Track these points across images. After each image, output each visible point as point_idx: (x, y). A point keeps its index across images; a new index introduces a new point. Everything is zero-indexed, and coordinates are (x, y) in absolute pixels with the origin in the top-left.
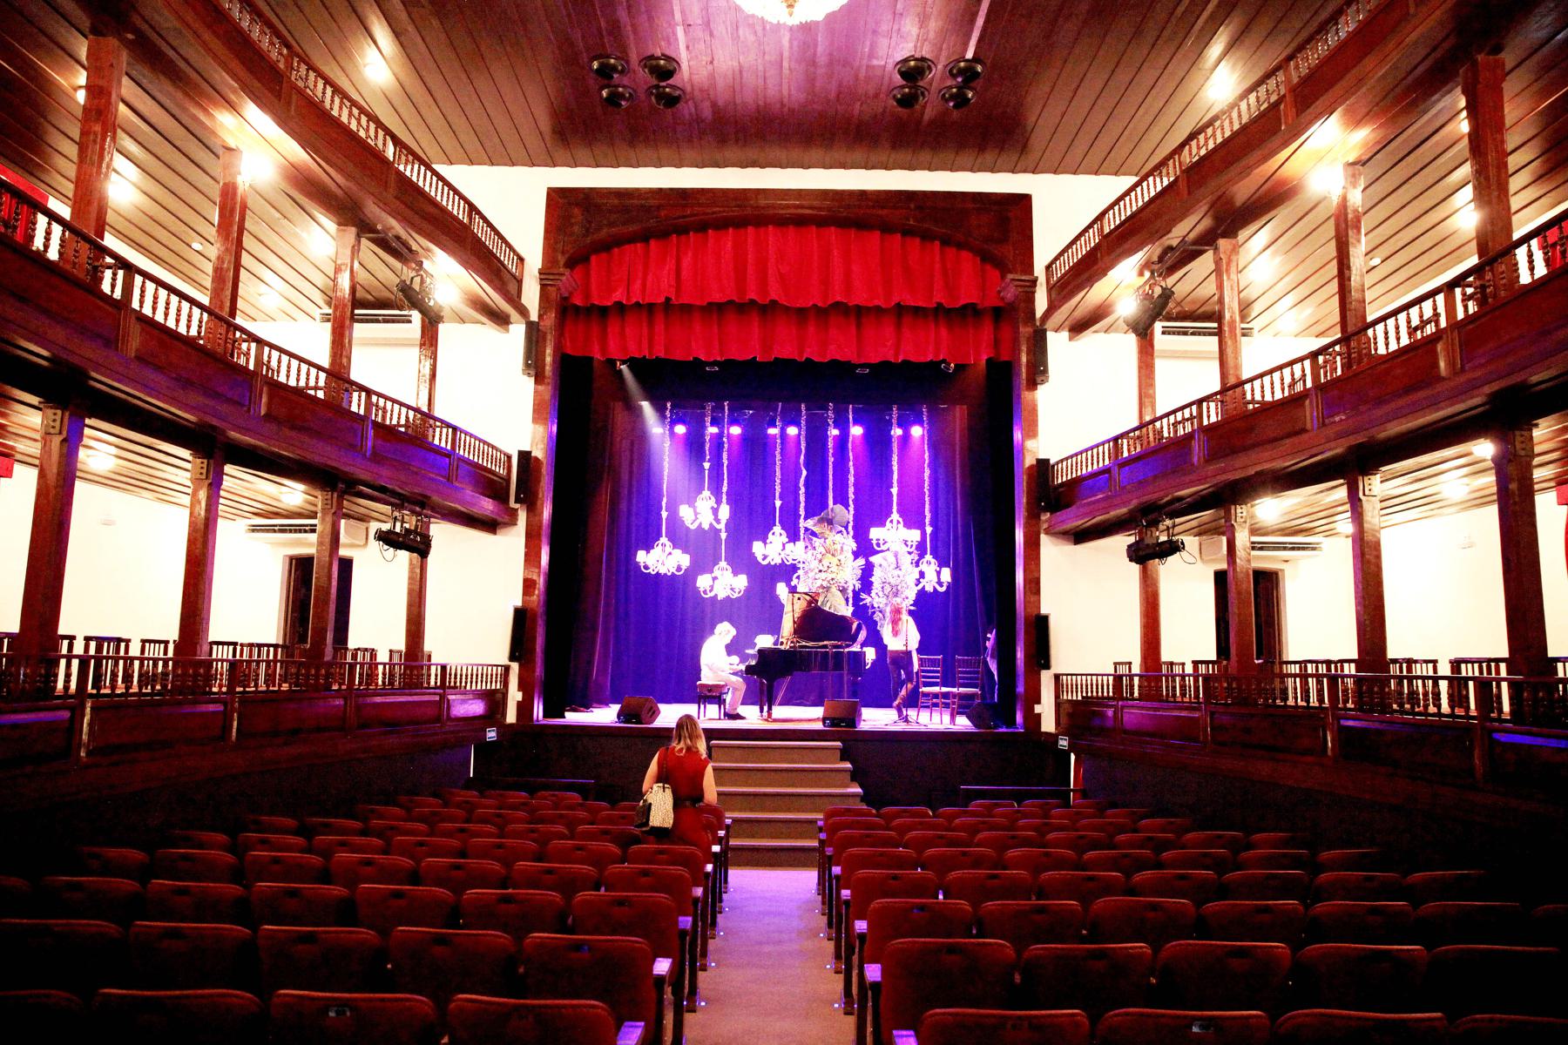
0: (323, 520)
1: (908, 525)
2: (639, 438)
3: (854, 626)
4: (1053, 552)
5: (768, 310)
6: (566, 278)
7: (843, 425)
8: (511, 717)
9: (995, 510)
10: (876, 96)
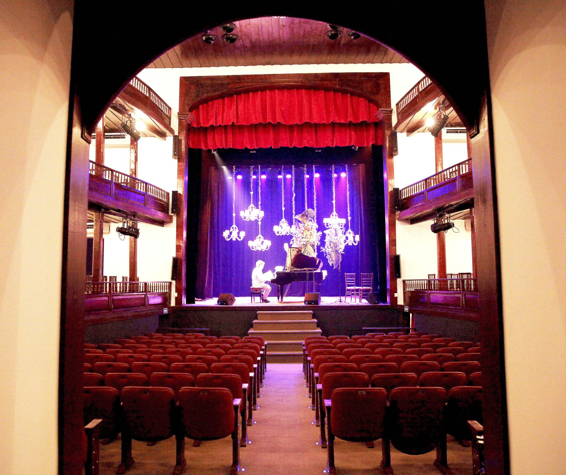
0: (96, 224)
1: (340, 216)
2: (222, 183)
3: (318, 261)
4: (402, 228)
5: (277, 126)
6: (190, 117)
7: (310, 173)
8: (173, 304)
9: (376, 209)
10: (320, 35)
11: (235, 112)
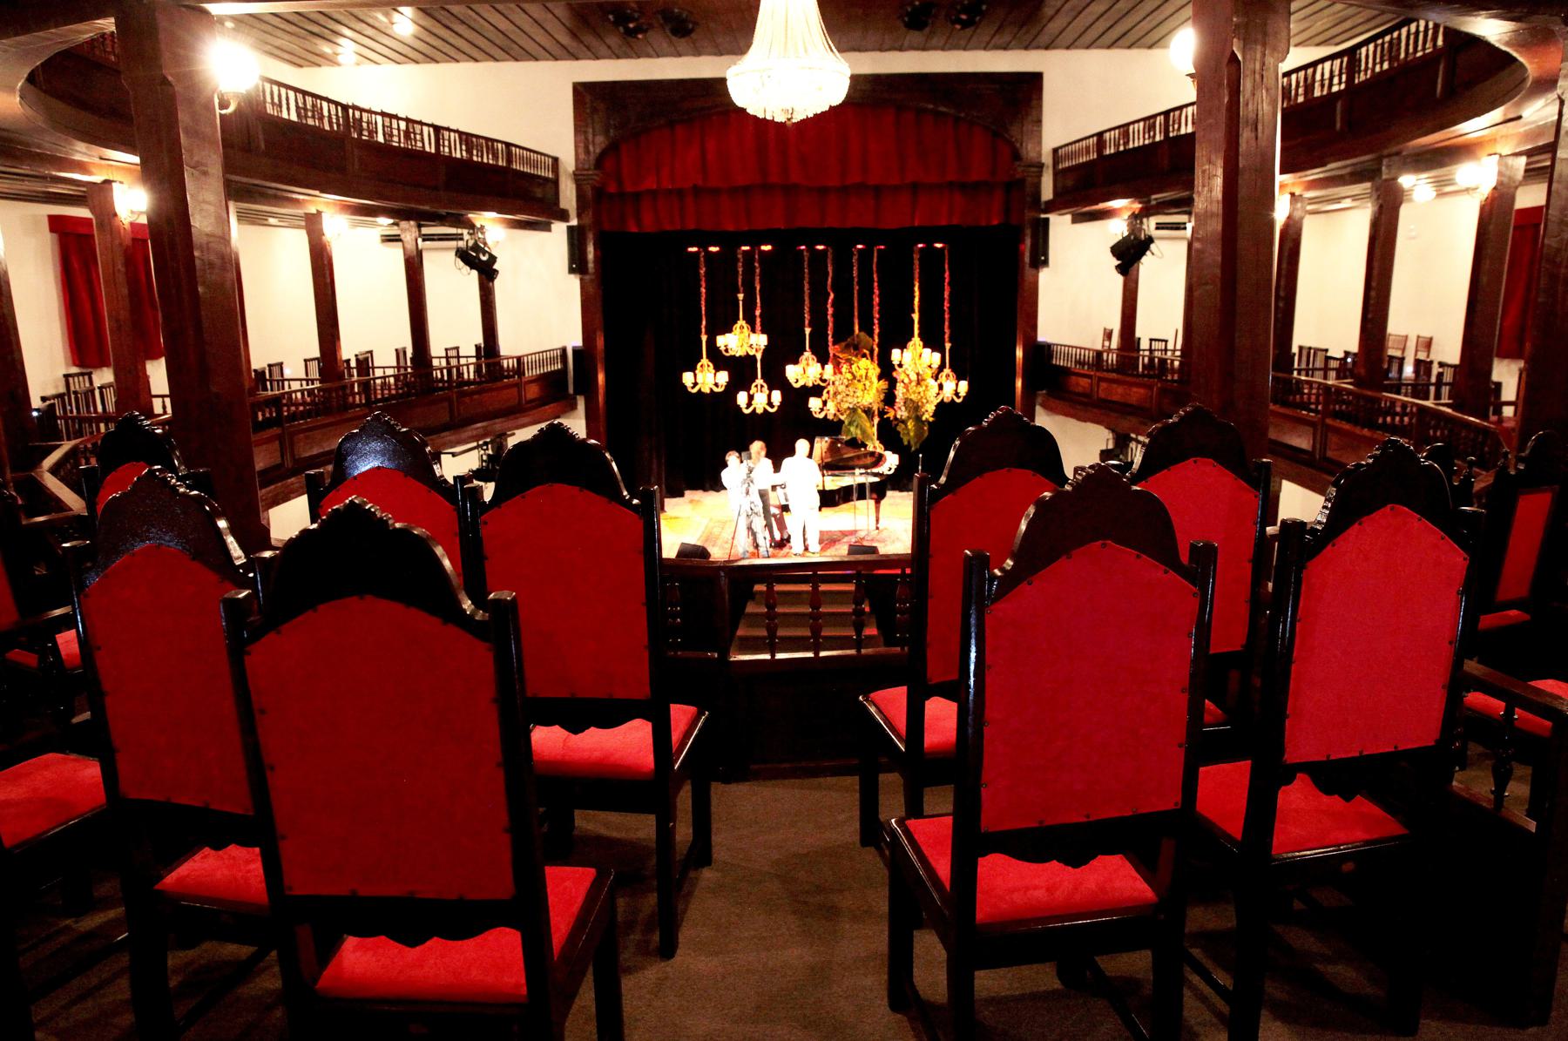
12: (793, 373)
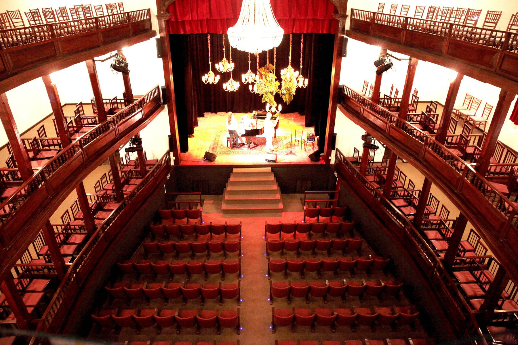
11: (208, 8)
12: (244, 77)
